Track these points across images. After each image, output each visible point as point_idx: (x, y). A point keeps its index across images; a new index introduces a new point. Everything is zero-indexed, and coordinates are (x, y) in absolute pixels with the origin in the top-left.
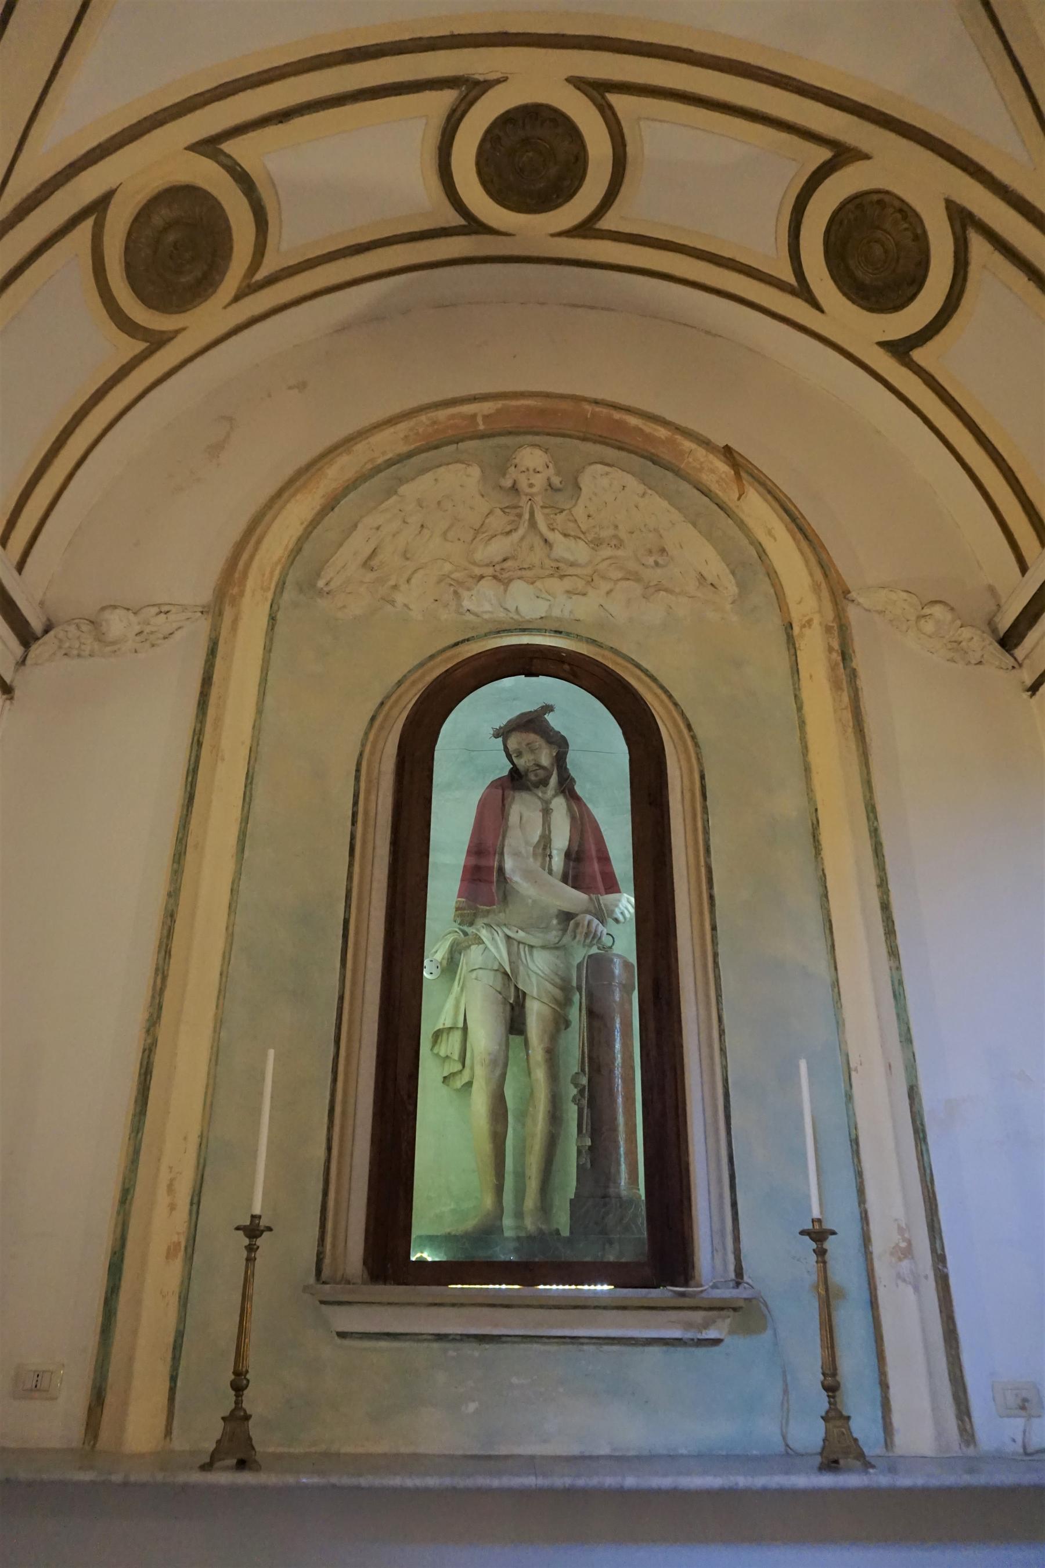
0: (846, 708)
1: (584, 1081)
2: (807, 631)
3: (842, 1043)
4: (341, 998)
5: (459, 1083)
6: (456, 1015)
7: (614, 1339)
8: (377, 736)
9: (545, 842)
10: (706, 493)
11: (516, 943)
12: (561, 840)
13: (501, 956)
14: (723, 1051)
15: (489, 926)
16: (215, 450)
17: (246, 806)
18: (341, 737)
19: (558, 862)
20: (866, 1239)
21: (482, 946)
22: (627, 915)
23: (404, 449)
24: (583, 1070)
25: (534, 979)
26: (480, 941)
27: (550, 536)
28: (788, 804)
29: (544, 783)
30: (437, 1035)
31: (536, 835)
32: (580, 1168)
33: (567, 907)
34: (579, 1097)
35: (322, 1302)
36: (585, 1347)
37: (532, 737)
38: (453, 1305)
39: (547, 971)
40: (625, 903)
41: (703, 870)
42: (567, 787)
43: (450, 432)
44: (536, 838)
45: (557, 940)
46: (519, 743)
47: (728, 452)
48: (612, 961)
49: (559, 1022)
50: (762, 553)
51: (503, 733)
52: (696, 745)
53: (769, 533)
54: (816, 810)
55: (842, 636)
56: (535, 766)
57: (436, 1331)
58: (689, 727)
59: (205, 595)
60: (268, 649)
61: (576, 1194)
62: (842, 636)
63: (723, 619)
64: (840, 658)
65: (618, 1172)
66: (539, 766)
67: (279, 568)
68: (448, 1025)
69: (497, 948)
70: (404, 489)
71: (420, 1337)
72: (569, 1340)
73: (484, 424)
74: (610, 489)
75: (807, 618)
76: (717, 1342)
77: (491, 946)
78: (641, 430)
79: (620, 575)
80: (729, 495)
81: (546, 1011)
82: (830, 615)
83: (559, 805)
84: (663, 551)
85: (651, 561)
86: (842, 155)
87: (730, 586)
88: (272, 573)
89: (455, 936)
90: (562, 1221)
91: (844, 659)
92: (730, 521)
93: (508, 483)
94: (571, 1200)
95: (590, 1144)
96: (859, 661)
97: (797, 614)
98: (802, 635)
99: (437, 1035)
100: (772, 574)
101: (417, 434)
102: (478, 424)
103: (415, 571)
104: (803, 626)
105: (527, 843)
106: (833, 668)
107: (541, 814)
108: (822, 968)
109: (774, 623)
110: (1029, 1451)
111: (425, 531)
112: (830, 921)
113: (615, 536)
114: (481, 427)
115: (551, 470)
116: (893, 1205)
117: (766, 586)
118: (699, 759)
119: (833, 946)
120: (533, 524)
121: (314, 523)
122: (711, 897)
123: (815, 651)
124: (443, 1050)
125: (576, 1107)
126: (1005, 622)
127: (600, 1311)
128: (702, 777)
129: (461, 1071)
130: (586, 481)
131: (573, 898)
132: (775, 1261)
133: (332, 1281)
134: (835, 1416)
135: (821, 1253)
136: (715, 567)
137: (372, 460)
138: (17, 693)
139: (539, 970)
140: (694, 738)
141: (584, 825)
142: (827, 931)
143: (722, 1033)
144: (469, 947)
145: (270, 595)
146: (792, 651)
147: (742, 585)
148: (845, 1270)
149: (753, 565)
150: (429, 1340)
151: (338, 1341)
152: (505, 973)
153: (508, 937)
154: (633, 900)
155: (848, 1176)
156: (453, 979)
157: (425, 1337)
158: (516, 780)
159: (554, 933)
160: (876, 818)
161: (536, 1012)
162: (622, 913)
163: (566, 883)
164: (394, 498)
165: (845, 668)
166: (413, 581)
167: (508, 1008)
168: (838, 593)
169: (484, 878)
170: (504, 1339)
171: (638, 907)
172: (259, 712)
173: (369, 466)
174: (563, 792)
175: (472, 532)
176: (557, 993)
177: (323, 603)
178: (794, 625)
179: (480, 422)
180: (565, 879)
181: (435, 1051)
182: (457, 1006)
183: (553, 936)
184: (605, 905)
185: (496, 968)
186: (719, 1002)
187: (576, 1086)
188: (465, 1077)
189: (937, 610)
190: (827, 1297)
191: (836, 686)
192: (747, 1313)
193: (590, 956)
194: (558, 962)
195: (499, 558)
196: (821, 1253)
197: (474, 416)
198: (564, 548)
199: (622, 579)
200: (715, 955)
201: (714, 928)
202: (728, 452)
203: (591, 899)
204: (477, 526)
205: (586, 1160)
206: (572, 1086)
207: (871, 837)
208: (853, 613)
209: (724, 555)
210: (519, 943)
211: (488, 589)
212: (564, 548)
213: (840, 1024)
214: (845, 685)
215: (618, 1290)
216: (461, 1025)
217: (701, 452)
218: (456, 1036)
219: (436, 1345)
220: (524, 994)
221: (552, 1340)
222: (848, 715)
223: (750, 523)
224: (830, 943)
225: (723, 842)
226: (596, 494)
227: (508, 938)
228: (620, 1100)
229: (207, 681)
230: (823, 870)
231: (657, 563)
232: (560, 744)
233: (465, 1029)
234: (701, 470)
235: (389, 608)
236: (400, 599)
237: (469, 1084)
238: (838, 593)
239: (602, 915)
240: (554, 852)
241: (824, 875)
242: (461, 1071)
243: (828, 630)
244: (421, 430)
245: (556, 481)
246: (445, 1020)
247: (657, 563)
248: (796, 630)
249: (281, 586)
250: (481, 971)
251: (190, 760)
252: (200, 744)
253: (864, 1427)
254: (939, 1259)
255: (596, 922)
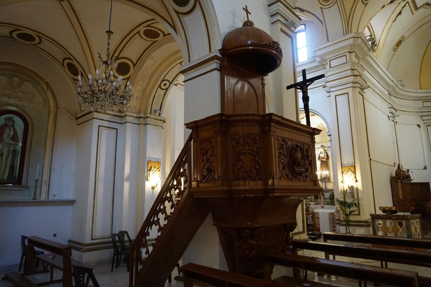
9: (9, 134)
10: (42, 89)
12: (12, 134)
20: (42, 181)
31: (8, 132)
50: (48, 100)
55: (56, 114)
62: (56, 114)
74: (28, 86)
80: (46, 91)
86: (139, 32)
100: (49, 105)
110: (94, 238)
116: (45, 178)
123: (52, 116)
126: (78, 116)
132: (31, 183)
134: (35, 196)
135: (36, 182)
136: (41, 101)
138: (55, 233)
141: (15, 132)
148: (39, 184)
149: (46, 101)
155: (41, 175)
168: (57, 107)
171: (22, 145)
180: (11, 139)
189: (69, 113)
190: (36, 187)
192: (27, 187)
196: (36, 182)
198: (19, 94)
208: (58, 110)
212: (19, 94)
232: (14, 122)
238: (57, 107)
239: (17, 145)
243: (54, 113)
253: (38, 197)
254: (49, 183)
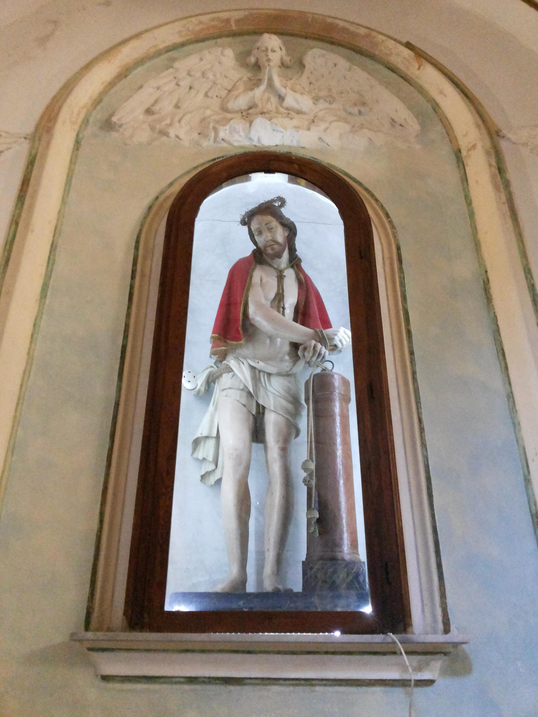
0: (504, 203)
1: (312, 466)
2: (472, 153)
3: (518, 440)
4: (117, 404)
5: (212, 480)
6: (211, 427)
7: (341, 680)
8: (153, 220)
9: (280, 297)
11: (257, 372)
12: (291, 299)
13: (246, 380)
14: (424, 445)
15: (237, 358)
16: (43, 41)
17: (50, 266)
18: (124, 214)
19: (289, 312)
21: (231, 374)
22: (344, 343)
23: (178, 40)
24: (311, 458)
25: (271, 398)
26: (229, 370)
27: (283, 91)
28: (464, 269)
29: (279, 255)
30: (197, 443)
32: (310, 536)
33: (296, 339)
34: (308, 479)
35: (89, 649)
36: (317, 688)
37: (269, 218)
38: (203, 651)
39: (282, 391)
40: (343, 335)
41: (401, 313)
42: (295, 262)
43: (211, 31)
44: (272, 295)
45: (288, 369)
46: (260, 223)
47: (409, 45)
48: (332, 376)
49: (290, 431)
50: (436, 107)
51: (247, 220)
52: (393, 227)
53: (441, 92)
54: (486, 272)
56: (272, 242)
57: (188, 675)
58: (387, 216)
59: (30, 129)
60: (73, 161)
61: (306, 559)
63: (409, 147)
64: (497, 171)
65: (341, 539)
66: (277, 243)
67: (84, 111)
68: (205, 434)
69: (242, 372)
70: (177, 65)
71: (174, 680)
72: (303, 682)
73: (236, 25)
75: (471, 145)
76: (430, 682)
77: (240, 370)
78: (348, 29)
79: (335, 118)
81: (281, 420)
82: (488, 143)
83: (290, 275)
84: (364, 104)
85: (355, 110)
87: (414, 126)
88: (79, 114)
89: (211, 369)
90: (296, 584)
91: (500, 172)
92: (411, 88)
93: (252, 60)
94: (303, 562)
95: (317, 516)
96: (512, 174)
97: (463, 144)
98: (468, 156)
99: (197, 443)
101: (188, 30)
102: (231, 25)
103: (184, 116)
104: (469, 150)
105: (266, 299)
106: (493, 176)
107: (276, 279)
108: (498, 383)
109: (445, 151)
111: (192, 90)
112: (503, 350)
113: (330, 96)
114: (234, 27)
115: (284, 51)
117: (439, 128)
118: (395, 237)
119: (506, 368)
120: (271, 85)
121: (112, 84)
122: (409, 332)
123: (479, 167)
124: (200, 454)
125: (306, 487)
127: (330, 656)
128: (398, 249)
129: (214, 470)
130: (308, 60)
131: (301, 332)
133: (99, 629)
136: (402, 113)
137: (155, 46)
139: (273, 395)
140: (391, 222)
142: (501, 357)
143: (422, 430)
144: (221, 375)
145: (77, 127)
146: (462, 167)
147: (423, 126)
149: (431, 113)
150: (180, 683)
151: (103, 684)
152: (249, 393)
153: (250, 365)
154: (349, 333)
156: (208, 404)
157: (177, 680)
158: (259, 257)
159: (287, 364)
160: (532, 278)
161: (272, 422)
162: (340, 341)
163: (297, 322)
164: (171, 70)
165: (501, 178)
166: (183, 121)
167: (251, 418)
168: (493, 134)
169: (233, 326)
170: (246, 681)
172: (64, 202)
173: (153, 50)
174: (292, 267)
175: (226, 92)
176: (290, 406)
177: (114, 135)
178: (462, 151)
179: (233, 25)
181: (195, 455)
182: (212, 421)
183: (286, 365)
184: (327, 335)
185: (242, 387)
186: (418, 407)
187: (305, 469)
188: (216, 476)
191: (496, 188)
193: (316, 375)
194: (290, 385)
195: (246, 108)
197: (228, 21)
199: (335, 121)
200: (414, 373)
201: (412, 353)
202: (409, 45)
203: (316, 332)
204: (229, 88)
205: (315, 529)
206: (303, 471)
207: (530, 291)
208: (503, 145)
209: (410, 108)
210: (260, 371)
211: (239, 124)
213: (516, 425)
214: (502, 190)
215: (345, 636)
216: (214, 434)
217: (391, 43)
218: (211, 443)
219: (186, 687)
220: (264, 408)
221: (287, 682)
222: (506, 208)
223: (427, 87)
224: (503, 365)
225: (415, 291)
226: (315, 69)
227: (253, 368)
228: (341, 482)
229: (25, 182)
230: (494, 313)
231: (360, 112)
233: (218, 437)
234: (391, 54)
235: (164, 138)
236: (172, 132)
237: (219, 482)
238: (493, 134)
240: (287, 306)
241: (496, 317)
242: (214, 470)
243: (487, 153)
244: (190, 28)
245: (287, 59)
246: (202, 430)
247: (360, 112)
248: (464, 153)
249: (86, 122)
250: (230, 391)
251: (9, 234)
252: (17, 224)
255: (319, 346)
